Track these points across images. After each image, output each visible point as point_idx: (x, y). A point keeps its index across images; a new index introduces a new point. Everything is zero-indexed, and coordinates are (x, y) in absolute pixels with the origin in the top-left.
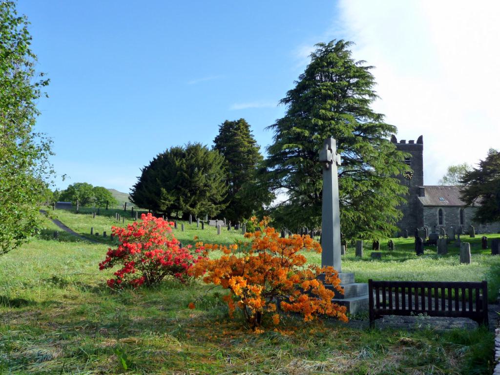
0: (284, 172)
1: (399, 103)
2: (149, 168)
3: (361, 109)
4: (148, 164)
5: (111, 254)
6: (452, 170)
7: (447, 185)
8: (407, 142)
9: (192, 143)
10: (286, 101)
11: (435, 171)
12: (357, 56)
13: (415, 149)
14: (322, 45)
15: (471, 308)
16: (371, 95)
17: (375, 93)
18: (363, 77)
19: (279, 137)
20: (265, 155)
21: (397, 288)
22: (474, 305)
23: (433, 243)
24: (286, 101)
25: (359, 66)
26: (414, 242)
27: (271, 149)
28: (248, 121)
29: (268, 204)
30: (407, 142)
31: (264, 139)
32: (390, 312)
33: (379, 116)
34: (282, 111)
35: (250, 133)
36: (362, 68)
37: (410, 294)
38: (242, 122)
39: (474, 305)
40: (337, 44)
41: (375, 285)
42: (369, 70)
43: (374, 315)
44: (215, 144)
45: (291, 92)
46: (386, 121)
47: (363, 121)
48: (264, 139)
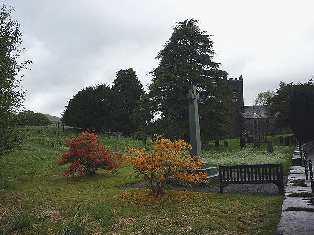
0: (159, 101)
1: (227, 57)
2: (73, 100)
3: (207, 60)
4: (72, 98)
5: (65, 157)
6: (261, 96)
7: (258, 105)
8: (233, 80)
9: (100, 84)
10: (159, 57)
11: (250, 99)
12: (203, 27)
13: (238, 84)
14: (180, 22)
15: (274, 178)
16: (211, 52)
17: (213, 52)
18: (206, 43)
19: (155, 79)
20: (147, 91)
21: (231, 170)
22: (276, 177)
23: (251, 141)
24: (159, 57)
25: (202, 34)
26: (60, 116)
27: (150, 87)
28: (135, 70)
29: (149, 120)
30: (233, 80)
31: (145, 80)
32: (231, 183)
33: (216, 65)
34: (157, 63)
35: (137, 77)
36: (206, 36)
37: (248, 172)
38: (131, 69)
39: (276, 177)
40: (190, 21)
41: (222, 168)
42: (209, 37)
43: (222, 183)
44: (114, 85)
45: (162, 52)
46: (220, 68)
47: (207, 68)
48: (145, 80)
